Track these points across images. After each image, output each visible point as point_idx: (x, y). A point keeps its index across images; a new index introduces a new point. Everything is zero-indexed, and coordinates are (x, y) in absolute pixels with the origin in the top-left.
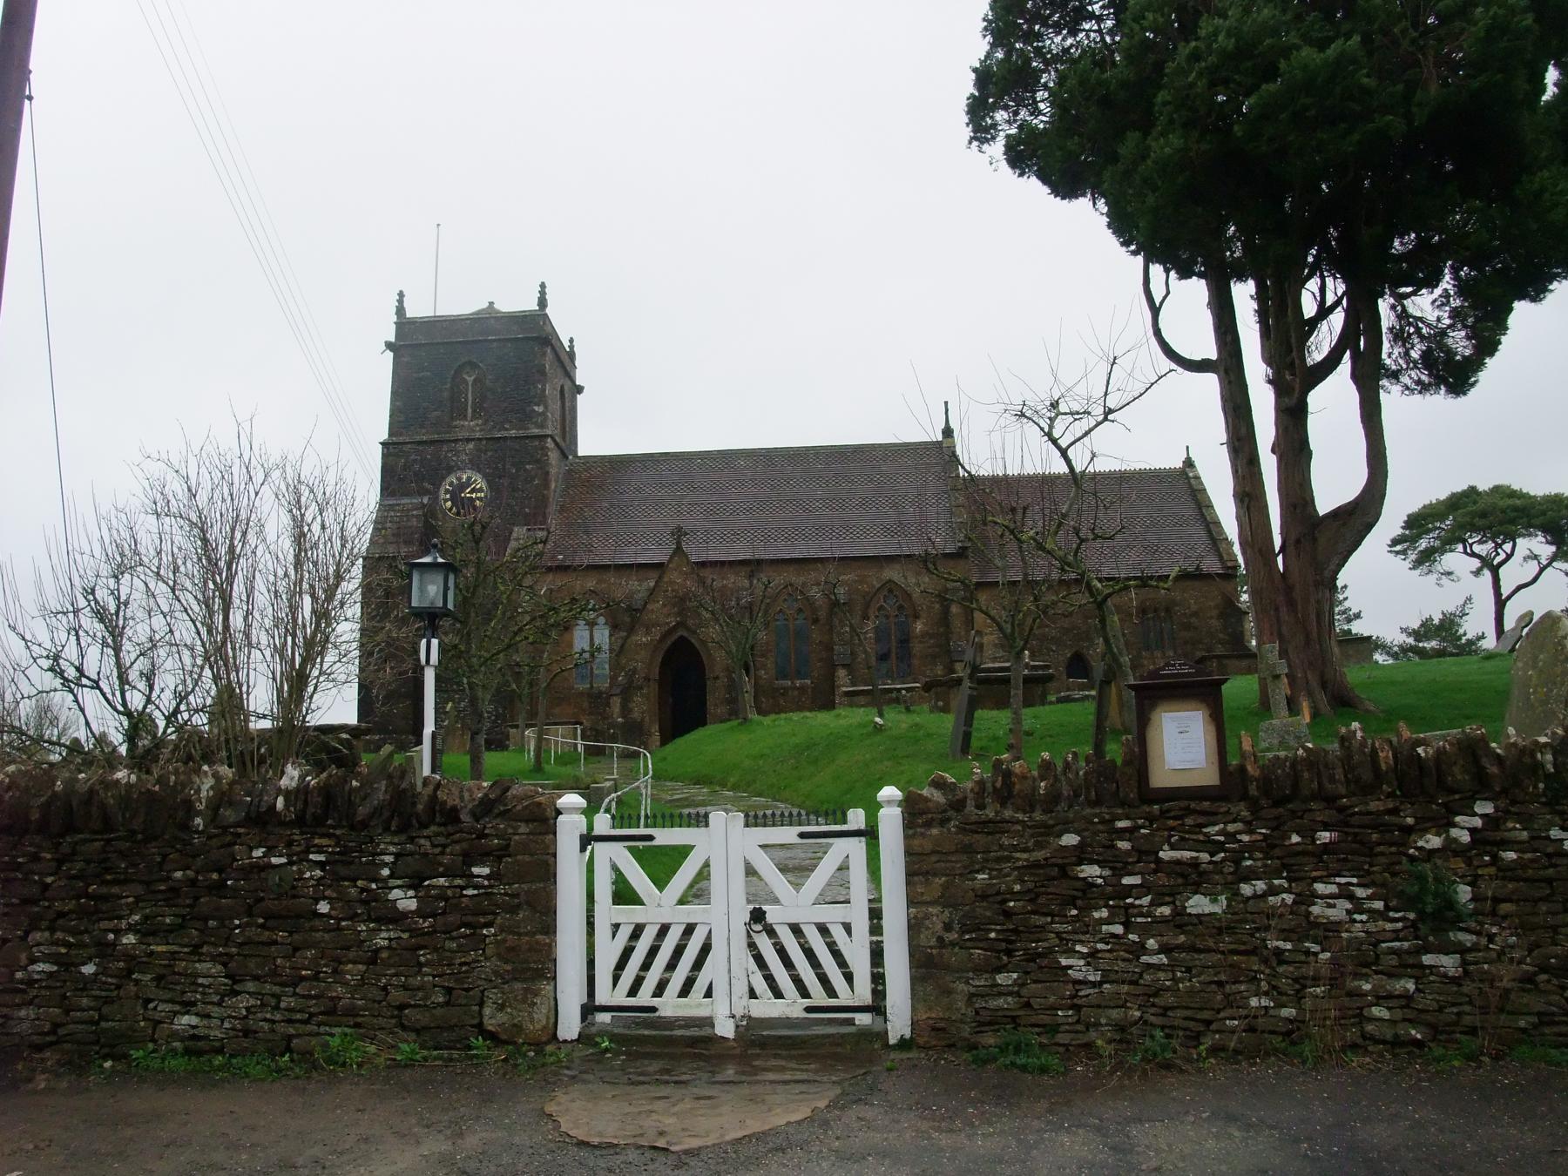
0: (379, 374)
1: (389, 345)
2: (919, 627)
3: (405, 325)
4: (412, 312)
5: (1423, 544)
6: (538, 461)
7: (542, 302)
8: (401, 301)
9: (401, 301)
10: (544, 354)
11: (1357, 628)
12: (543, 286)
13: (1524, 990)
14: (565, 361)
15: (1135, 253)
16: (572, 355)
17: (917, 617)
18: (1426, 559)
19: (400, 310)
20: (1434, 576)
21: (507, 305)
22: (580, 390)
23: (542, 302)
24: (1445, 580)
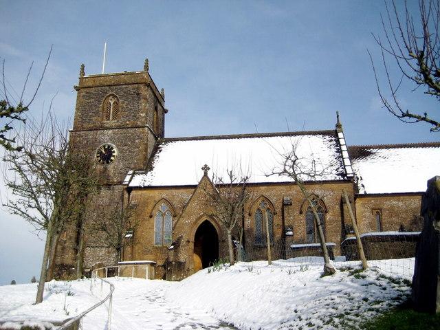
7: (146, 67)
12: (147, 60)
23: (146, 67)
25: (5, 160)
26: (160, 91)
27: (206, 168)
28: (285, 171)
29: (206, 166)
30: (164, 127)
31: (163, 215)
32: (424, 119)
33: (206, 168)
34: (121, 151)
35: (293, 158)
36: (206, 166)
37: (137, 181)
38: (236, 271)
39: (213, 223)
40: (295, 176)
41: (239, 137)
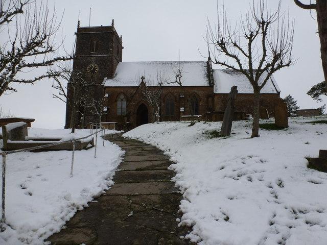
0: (74, 38)
1: (76, 33)
2: (201, 103)
3: (79, 29)
4: (82, 25)
5: (315, 92)
6: (111, 62)
7: (113, 24)
8: (79, 23)
9: (79, 23)
10: (113, 36)
11: (300, 109)
12: (113, 20)
13: (71, 238)
14: (119, 41)
15: (189, 228)
16: (121, 39)
17: (201, 101)
18: (316, 95)
19: (78, 26)
20: (316, 100)
21: (105, 25)
22: (123, 48)
23: (113, 24)
24: (319, 101)
25: (53, 86)
26: (120, 37)
27: (143, 78)
28: (176, 82)
29: (143, 77)
30: (111, 87)
31: (122, 100)
32: (224, 64)
33: (143, 78)
34: (100, 68)
35: (180, 76)
36: (143, 77)
37: (108, 83)
38: (258, 156)
39: (146, 104)
40: (180, 84)
41: (4, 190)
